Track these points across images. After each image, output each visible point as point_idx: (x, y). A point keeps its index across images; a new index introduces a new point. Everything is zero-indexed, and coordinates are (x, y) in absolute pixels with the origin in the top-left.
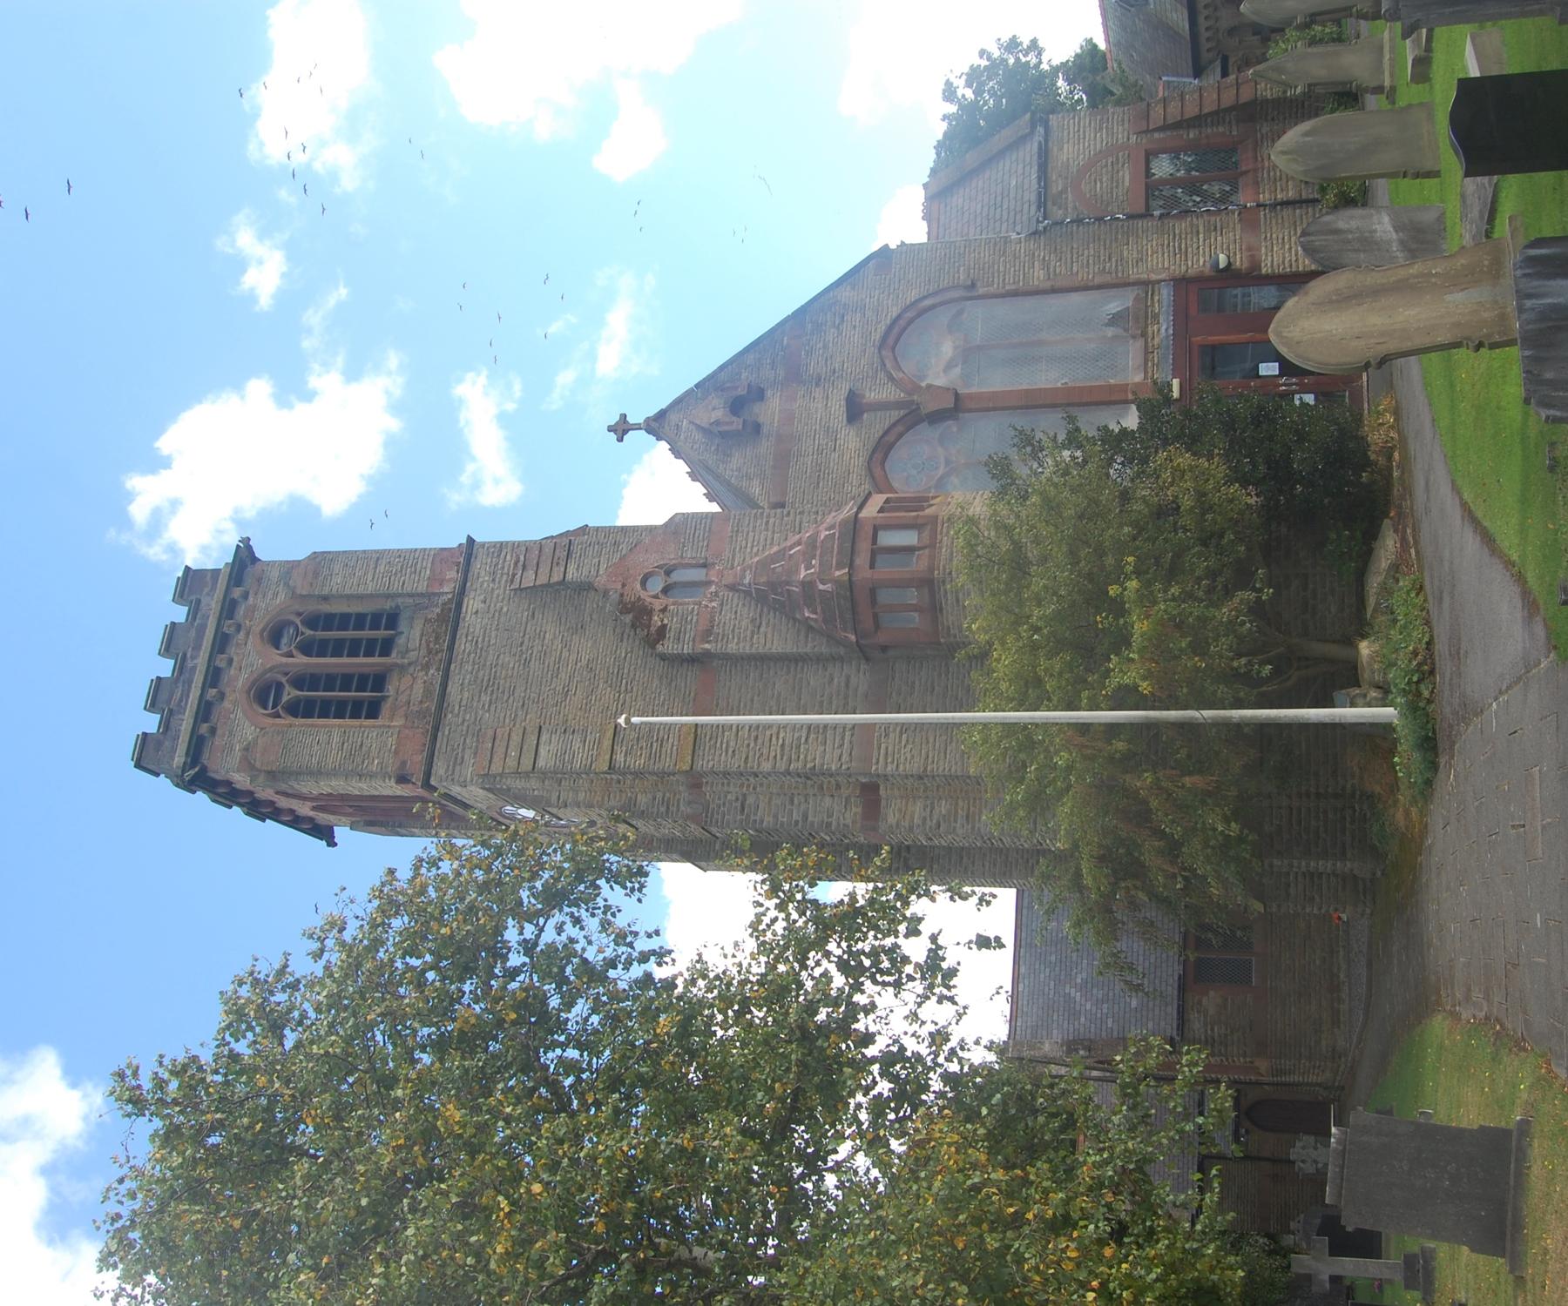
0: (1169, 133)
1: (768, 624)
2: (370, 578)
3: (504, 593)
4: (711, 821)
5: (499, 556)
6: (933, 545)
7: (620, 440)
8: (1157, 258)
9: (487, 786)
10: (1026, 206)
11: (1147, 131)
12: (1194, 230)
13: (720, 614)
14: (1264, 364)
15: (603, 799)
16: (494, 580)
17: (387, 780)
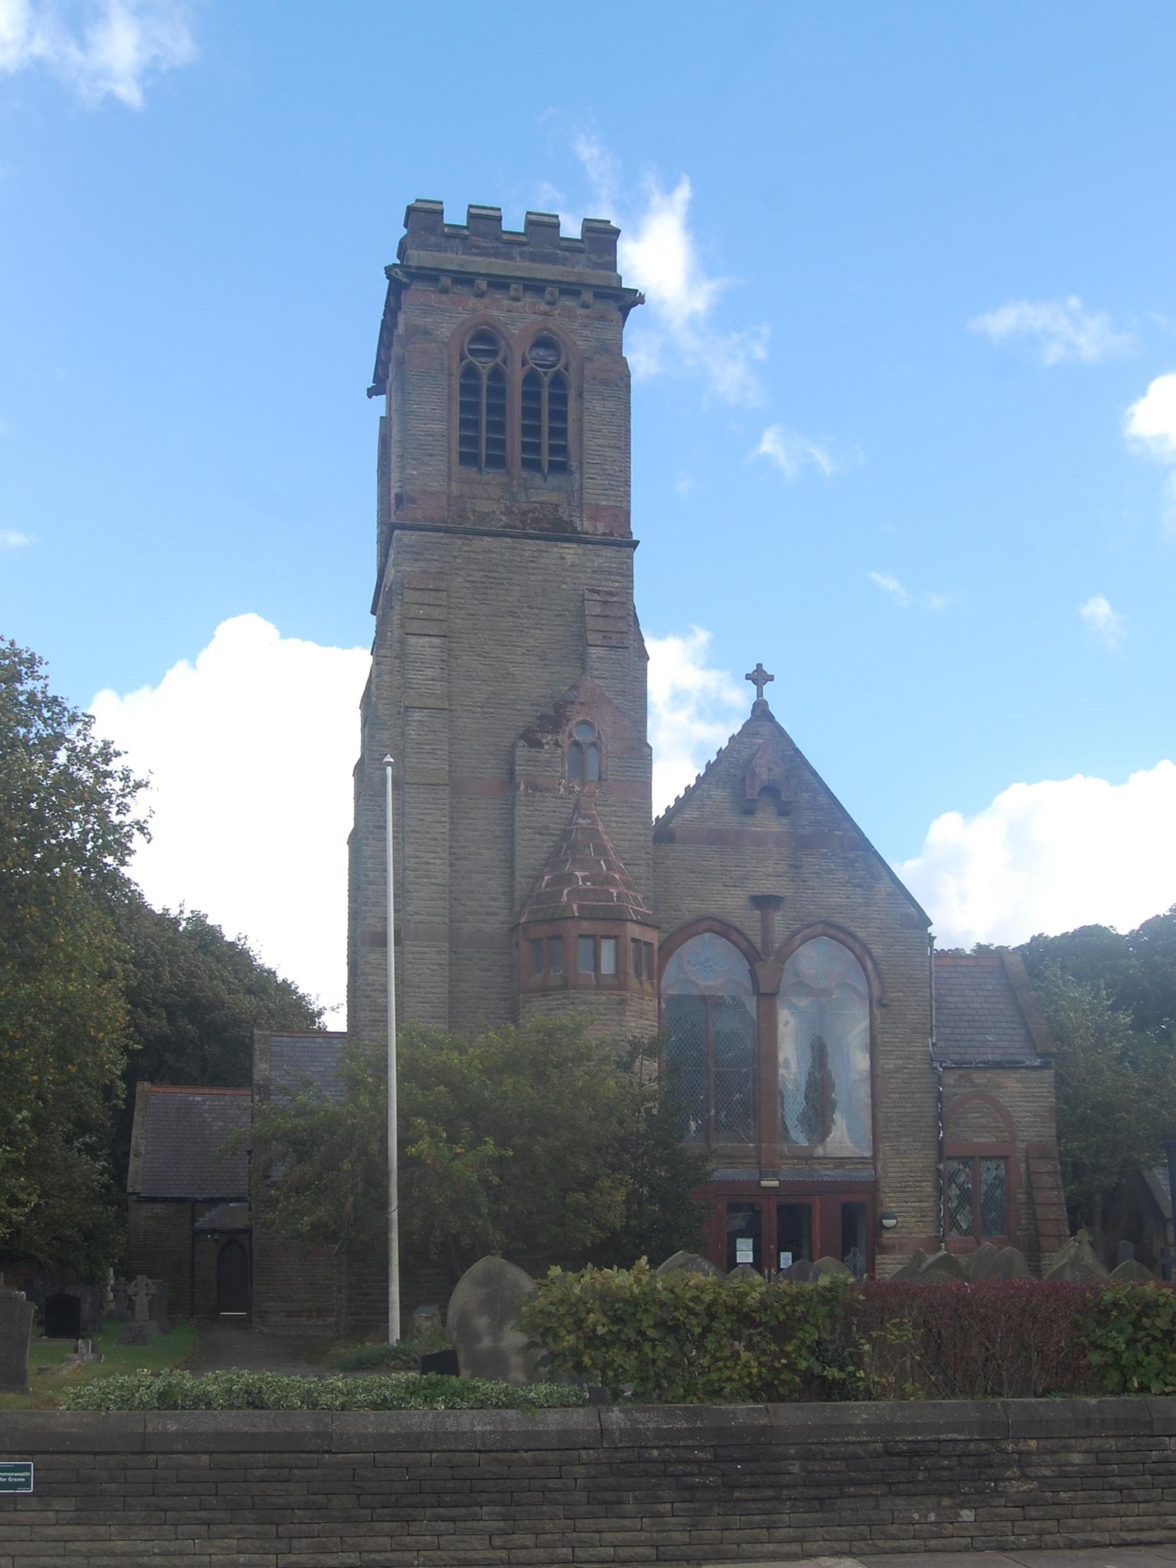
0: (1024, 1176)
1: (542, 841)
2: (599, 442)
3: (582, 584)
4: (366, 800)
5: (619, 574)
6: (600, 985)
7: (748, 677)
8: (898, 1167)
9: (393, 587)
10: (962, 1051)
11: (1027, 1158)
12: (922, 1199)
13: (552, 797)
14: (790, 1257)
15: (385, 698)
16: (594, 572)
17: (398, 484)
